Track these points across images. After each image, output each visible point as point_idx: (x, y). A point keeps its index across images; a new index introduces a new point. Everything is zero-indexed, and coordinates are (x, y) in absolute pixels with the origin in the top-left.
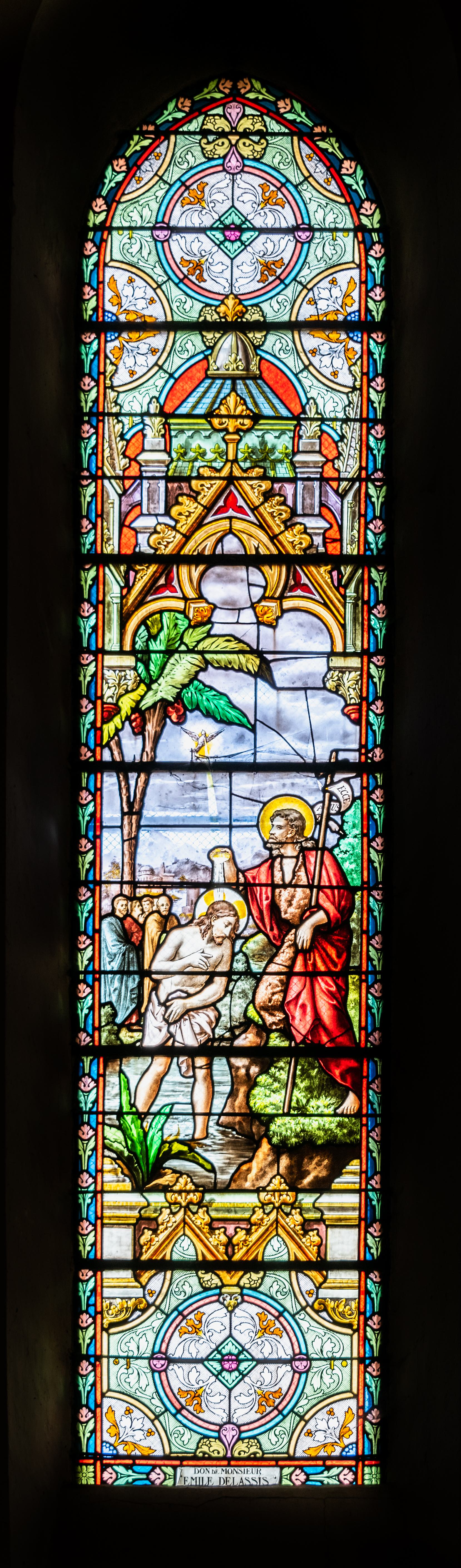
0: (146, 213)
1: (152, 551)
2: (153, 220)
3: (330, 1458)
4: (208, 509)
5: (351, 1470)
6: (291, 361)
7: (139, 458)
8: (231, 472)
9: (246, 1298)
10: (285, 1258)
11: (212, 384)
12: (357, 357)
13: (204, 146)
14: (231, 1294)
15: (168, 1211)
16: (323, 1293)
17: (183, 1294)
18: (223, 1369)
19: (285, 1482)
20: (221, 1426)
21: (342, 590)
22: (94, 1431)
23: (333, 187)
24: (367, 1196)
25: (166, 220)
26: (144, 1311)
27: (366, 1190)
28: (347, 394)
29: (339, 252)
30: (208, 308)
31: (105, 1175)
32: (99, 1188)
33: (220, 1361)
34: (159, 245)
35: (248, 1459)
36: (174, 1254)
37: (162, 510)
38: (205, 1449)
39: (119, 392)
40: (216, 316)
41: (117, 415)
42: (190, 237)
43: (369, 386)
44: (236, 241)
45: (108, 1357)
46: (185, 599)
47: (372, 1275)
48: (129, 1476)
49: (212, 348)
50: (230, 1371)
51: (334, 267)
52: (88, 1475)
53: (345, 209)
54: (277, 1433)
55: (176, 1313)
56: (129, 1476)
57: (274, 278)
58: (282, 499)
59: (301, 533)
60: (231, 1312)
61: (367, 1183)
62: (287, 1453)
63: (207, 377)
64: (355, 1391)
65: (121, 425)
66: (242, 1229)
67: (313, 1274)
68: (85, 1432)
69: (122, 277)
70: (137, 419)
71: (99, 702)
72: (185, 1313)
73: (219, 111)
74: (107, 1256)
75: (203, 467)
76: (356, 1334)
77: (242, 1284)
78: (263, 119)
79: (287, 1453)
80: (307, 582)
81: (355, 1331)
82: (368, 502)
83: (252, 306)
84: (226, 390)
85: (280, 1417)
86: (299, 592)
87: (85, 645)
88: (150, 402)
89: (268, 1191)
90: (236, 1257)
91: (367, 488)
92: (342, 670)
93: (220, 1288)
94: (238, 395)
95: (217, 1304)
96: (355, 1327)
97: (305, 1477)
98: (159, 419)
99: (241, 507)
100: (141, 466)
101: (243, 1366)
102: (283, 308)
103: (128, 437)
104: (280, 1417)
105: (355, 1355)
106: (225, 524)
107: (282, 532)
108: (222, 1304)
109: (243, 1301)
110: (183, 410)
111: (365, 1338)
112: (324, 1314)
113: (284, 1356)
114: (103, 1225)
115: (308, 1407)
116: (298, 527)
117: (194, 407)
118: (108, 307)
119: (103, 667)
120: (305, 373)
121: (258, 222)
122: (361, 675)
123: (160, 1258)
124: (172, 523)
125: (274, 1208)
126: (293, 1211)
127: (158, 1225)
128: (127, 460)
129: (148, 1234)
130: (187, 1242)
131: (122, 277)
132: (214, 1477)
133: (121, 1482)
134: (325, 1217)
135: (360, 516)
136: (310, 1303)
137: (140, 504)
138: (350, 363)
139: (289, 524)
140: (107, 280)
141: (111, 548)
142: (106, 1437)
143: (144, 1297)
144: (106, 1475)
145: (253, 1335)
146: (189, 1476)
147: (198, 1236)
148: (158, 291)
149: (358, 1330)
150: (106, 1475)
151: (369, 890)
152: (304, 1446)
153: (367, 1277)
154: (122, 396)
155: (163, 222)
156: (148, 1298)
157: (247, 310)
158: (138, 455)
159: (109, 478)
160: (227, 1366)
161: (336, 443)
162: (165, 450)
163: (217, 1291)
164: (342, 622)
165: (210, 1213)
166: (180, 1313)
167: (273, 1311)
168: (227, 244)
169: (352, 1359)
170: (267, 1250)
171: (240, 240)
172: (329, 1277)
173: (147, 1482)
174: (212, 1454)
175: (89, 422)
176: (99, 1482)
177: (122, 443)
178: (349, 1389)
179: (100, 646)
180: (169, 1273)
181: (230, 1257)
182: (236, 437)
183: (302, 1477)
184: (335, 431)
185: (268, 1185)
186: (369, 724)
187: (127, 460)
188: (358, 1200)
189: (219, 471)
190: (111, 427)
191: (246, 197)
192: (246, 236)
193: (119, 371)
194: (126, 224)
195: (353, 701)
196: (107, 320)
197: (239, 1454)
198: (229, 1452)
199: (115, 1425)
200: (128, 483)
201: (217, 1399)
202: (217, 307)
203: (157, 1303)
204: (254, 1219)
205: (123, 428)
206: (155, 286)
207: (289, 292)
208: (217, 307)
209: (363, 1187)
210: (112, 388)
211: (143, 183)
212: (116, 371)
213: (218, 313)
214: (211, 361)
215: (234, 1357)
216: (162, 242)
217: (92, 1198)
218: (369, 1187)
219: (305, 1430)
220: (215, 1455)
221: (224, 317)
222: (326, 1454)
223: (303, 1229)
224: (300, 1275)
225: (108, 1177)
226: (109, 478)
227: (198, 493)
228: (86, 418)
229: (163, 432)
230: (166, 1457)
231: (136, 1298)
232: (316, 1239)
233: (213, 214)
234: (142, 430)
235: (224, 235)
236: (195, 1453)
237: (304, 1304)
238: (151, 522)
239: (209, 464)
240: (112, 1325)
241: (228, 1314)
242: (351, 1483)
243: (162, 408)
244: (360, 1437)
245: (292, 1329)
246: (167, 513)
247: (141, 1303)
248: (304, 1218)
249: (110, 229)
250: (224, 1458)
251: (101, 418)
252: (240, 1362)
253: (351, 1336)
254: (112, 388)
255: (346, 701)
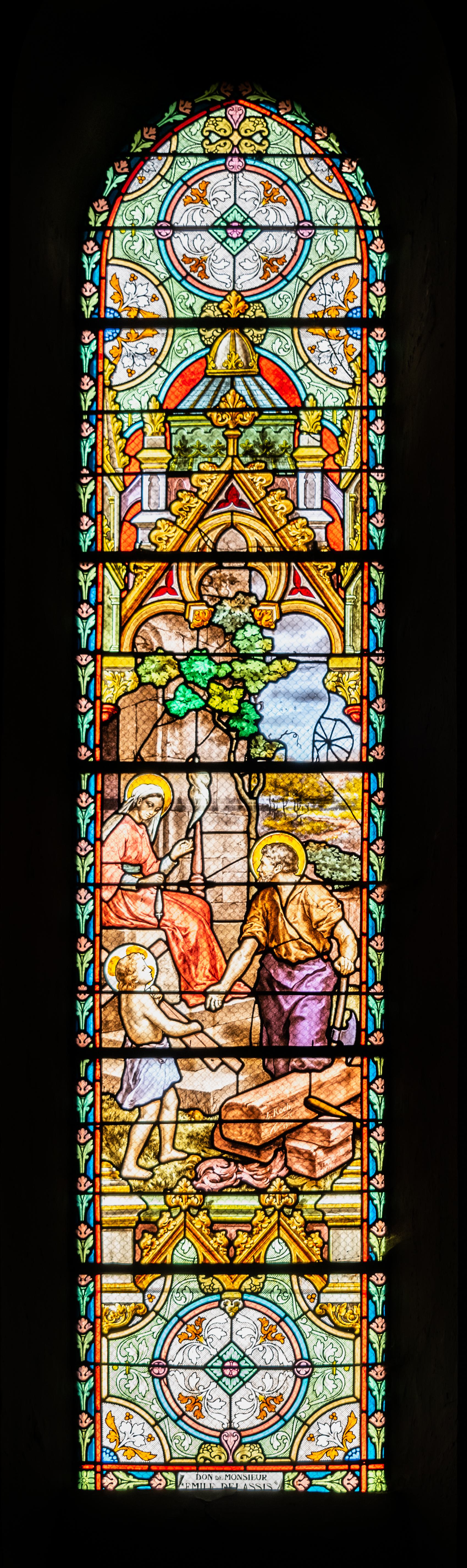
0: (149, 212)
1: (153, 548)
2: (155, 218)
3: (333, 1463)
4: (208, 505)
5: (355, 1475)
6: (290, 359)
7: (138, 456)
8: (232, 466)
9: (247, 1303)
10: (287, 1260)
11: (210, 383)
12: (356, 353)
13: (265, 129)
14: (232, 1300)
15: (168, 1215)
16: (324, 1298)
17: (183, 1299)
18: (224, 1375)
19: (288, 1488)
20: (222, 1432)
21: (342, 592)
22: (93, 1437)
23: (335, 184)
24: (370, 1199)
25: (168, 219)
26: (144, 1316)
27: (368, 1191)
28: (347, 390)
29: (341, 248)
30: (210, 305)
31: (103, 1179)
32: (97, 1190)
33: (223, 1368)
34: (161, 243)
35: (249, 1463)
36: (175, 1257)
37: (162, 506)
38: (207, 1454)
39: (118, 392)
40: (218, 312)
41: (116, 413)
42: (192, 234)
43: (369, 381)
44: (238, 238)
45: (108, 1364)
46: (184, 601)
47: (373, 1278)
48: (130, 1482)
49: (210, 347)
50: (231, 1377)
51: (334, 264)
52: (87, 1480)
53: (346, 205)
54: (279, 1437)
55: (176, 1319)
56: (130, 1482)
57: (276, 274)
58: (284, 492)
59: (303, 527)
60: (232, 1318)
61: (369, 1184)
62: (289, 1457)
63: (206, 376)
64: (357, 1394)
65: (120, 423)
66: (243, 1231)
67: (316, 1278)
68: (85, 1438)
69: (124, 275)
70: (136, 417)
71: (98, 702)
72: (185, 1319)
73: (221, 113)
74: (106, 1260)
75: (204, 462)
76: (359, 1338)
77: (243, 1289)
78: (265, 121)
79: (289, 1457)
80: (307, 585)
81: (357, 1336)
82: (369, 1015)
83: (254, 302)
84: (225, 388)
85: (282, 1422)
86: (299, 595)
87: (84, 645)
88: (150, 400)
89: (269, 1193)
90: (237, 1261)
91: (367, 1001)
92: (342, 670)
93: (220, 1293)
94: (237, 392)
95: (218, 1309)
96: (357, 1332)
97: (308, 1482)
98: (159, 415)
99: (242, 501)
100: (141, 463)
101: (243, 1373)
102: (285, 304)
103: (127, 435)
104: (282, 1422)
105: (358, 1361)
106: (226, 518)
107: (283, 527)
108: (224, 1310)
109: (244, 1306)
110: (185, 405)
111: (369, 1342)
112: (326, 1319)
113: (286, 1364)
114: (102, 1228)
115: (311, 1412)
116: (300, 521)
117: (197, 401)
118: (110, 303)
119: (102, 668)
120: (304, 370)
121: (261, 220)
122: (362, 674)
123: (159, 1262)
124: (174, 518)
125: (275, 1209)
126: (295, 1213)
127: (159, 1229)
128: (127, 458)
129: (148, 1239)
130: (187, 1245)
131: (124, 275)
132: (216, 1481)
133: (123, 1487)
134: (326, 1218)
135: (360, 509)
136: (312, 1308)
137: (140, 501)
138: (350, 360)
139: (290, 518)
140: (109, 278)
141: (111, 546)
142: (106, 1443)
143: (144, 1302)
144: (106, 1481)
145: (255, 1341)
146: (190, 1481)
147: (198, 1239)
148: (161, 288)
149: (360, 1335)
150: (106, 1481)
151: (369, 471)
152: (306, 1451)
153: (368, 1280)
154: (120, 394)
155: (165, 221)
156: (147, 1302)
157: (250, 307)
158: (138, 453)
159: (109, 475)
160: (227, 1372)
161: (337, 438)
162: (165, 448)
163: (217, 1297)
164: (342, 625)
165: (211, 1215)
166: (180, 1319)
167: (274, 1316)
168: (229, 241)
169: (354, 1365)
170: (269, 1252)
171: (242, 237)
172: (331, 1280)
173: (149, 1487)
174: (213, 1460)
175: (88, 421)
176: (99, 1488)
177: (122, 443)
178: (351, 1393)
179: (99, 647)
180: (169, 1277)
181: (232, 1259)
182: (238, 433)
183: (306, 1482)
184: (335, 425)
185: (269, 1187)
186: (370, 722)
187: (127, 458)
188: (359, 1201)
189: (219, 467)
190: (111, 425)
191: (248, 196)
192: (248, 234)
193: (117, 371)
194: (128, 224)
195: (353, 701)
196: (109, 316)
197: (242, 1458)
198: (231, 1457)
199: (116, 1431)
200: (128, 479)
201: (217, 1404)
202: (220, 303)
203: (157, 1308)
204: (255, 1221)
205: (122, 426)
206: (157, 283)
207: (291, 287)
208: (220, 303)
209: (365, 1187)
210: (111, 387)
211: (145, 182)
212: (115, 370)
213: (221, 310)
214: (210, 360)
215: (235, 1364)
216: (165, 240)
217: (89, 1202)
218: (372, 1188)
219: (307, 1435)
220: (217, 1460)
221: (226, 314)
222: (328, 1459)
223: (305, 1231)
224: (302, 1279)
225: (106, 1181)
226: (109, 475)
227: (199, 489)
228: (85, 417)
229: (163, 430)
230: (166, 1464)
231: (135, 1304)
232: (318, 1241)
233: (215, 212)
234: (142, 428)
235: (227, 233)
236: (196, 1458)
237: (306, 1309)
238: (151, 518)
239: (209, 460)
240: (112, 1330)
241: (229, 1320)
242: (355, 1488)
243: (161, 405)
244: (364, 1440)
245: (294, 1334)
246: (168, 508)
247: (140, 1308)
248: (305, 1219)
249: (113, 229)
250: (226, 1463)
251: (100, 416)
252: (240, 1368)
253: (354, 1340)
254: (111, 387)
255: (346, 702)
